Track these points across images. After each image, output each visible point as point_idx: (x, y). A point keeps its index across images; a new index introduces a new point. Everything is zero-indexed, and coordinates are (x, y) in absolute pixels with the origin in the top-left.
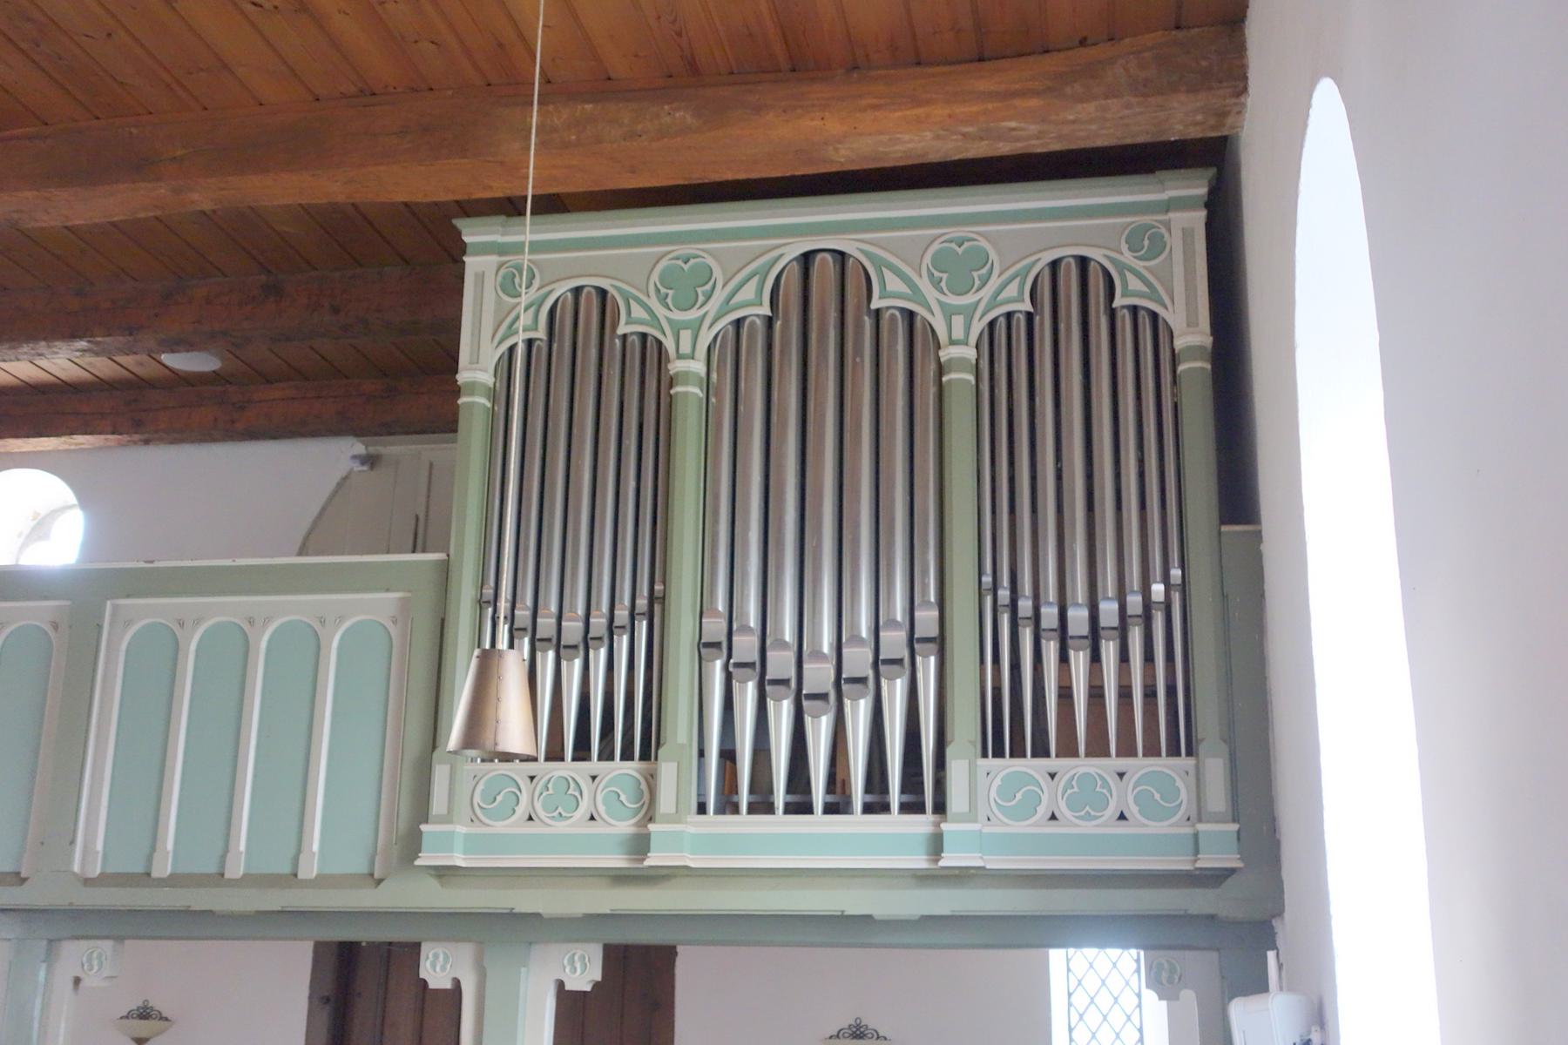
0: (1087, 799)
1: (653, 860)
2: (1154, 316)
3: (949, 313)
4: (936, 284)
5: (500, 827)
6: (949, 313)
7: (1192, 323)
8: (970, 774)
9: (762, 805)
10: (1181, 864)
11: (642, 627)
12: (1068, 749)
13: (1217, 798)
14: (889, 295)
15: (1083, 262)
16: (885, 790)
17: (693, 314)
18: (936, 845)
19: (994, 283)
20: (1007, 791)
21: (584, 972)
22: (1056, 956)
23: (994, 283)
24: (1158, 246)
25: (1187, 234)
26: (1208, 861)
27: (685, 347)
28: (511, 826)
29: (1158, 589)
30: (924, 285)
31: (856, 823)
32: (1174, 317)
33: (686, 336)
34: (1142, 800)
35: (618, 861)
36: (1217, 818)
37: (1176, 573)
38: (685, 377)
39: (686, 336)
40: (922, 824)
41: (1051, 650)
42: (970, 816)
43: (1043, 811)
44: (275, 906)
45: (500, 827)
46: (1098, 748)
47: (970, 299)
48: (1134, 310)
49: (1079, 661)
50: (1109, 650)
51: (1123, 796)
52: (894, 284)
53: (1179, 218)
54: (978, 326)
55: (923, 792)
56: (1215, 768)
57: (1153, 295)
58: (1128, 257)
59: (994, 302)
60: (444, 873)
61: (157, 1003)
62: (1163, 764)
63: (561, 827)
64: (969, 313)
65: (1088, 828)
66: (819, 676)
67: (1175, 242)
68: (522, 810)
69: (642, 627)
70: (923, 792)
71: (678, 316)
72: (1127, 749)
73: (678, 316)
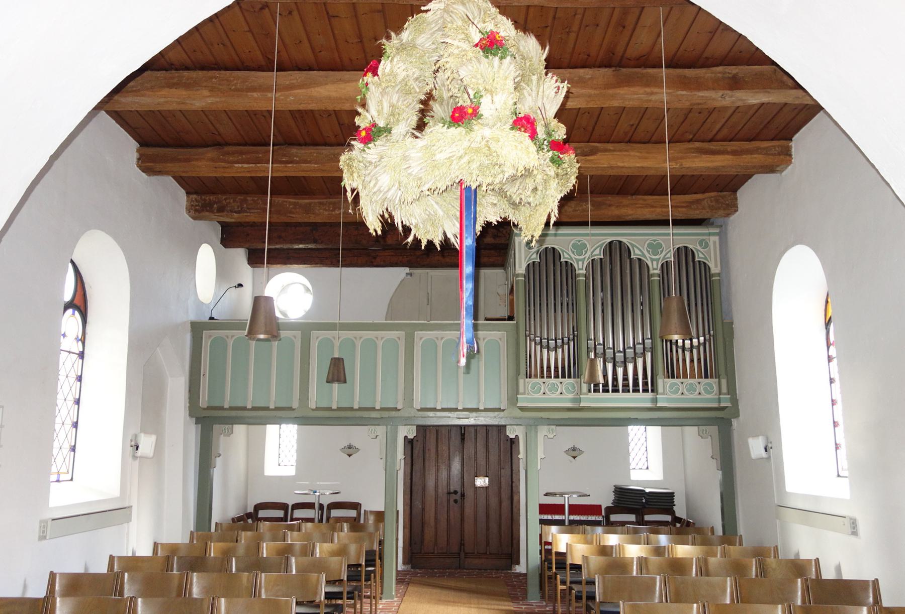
0: (691, 389)
1: (659, 405)
2: (705, 263)
3: (652, 260)
4: (649, 252)
5: (536, 396)
6: (652, 260)
7: (716, 266)
8: (663, 383)
9: (615, 390)
10: (715, 405)
11: (572, 343)
12: (685, 376)
13: (724, 390)
14: (635, 254)
15: (686, 248)
16: (638, 386)
17: (582, 257)
18: (655, 400)
19: (664, 253)
20: (672, 386)
21: (411, 432)
22: (630, 428)
23: (664, 253)
24: (707, 245)
25: (715, 243)
26: (723, 405)
27: (580, 267)
28: (539, 396)
29: (707, 336)
30: (645, 252)
31: (631, 395)
32: (711, 265)
33: (580, 263)
34: (705, 389)
35: (649, 405)
36: (725, 394)
37: (712, 332)
38: (579, 275)
39: (580, 263)
40: (649, 395)
41: (680, 351)
42: (663, 394)
43: (680, 392)
44: (656, 417)
45: (536, 396)
46: (557, 377)
47: (582, 257)
48: (699, 262)
49: (687, 354)
50: (695, 351)
51: (700, 388)
52: (637, 252)
53: (713, 238)
54: (660, 265)
55: (651, 386)
56: (724, 382)
57: (706, 258)
58: (699, 248)
59: (664, 258)
60: (522, 409)
61: (354, 444)
62: (571, 380)
63: (553, 396)
64: (657, 260)
65: (692, 396)
66: (620, 356)
67: (711, 244)
68: (542, 391)
69: (572, 343)
70: (651, 386)
71: (578, 257)
72: (563, 377)
73: (578, 257)
